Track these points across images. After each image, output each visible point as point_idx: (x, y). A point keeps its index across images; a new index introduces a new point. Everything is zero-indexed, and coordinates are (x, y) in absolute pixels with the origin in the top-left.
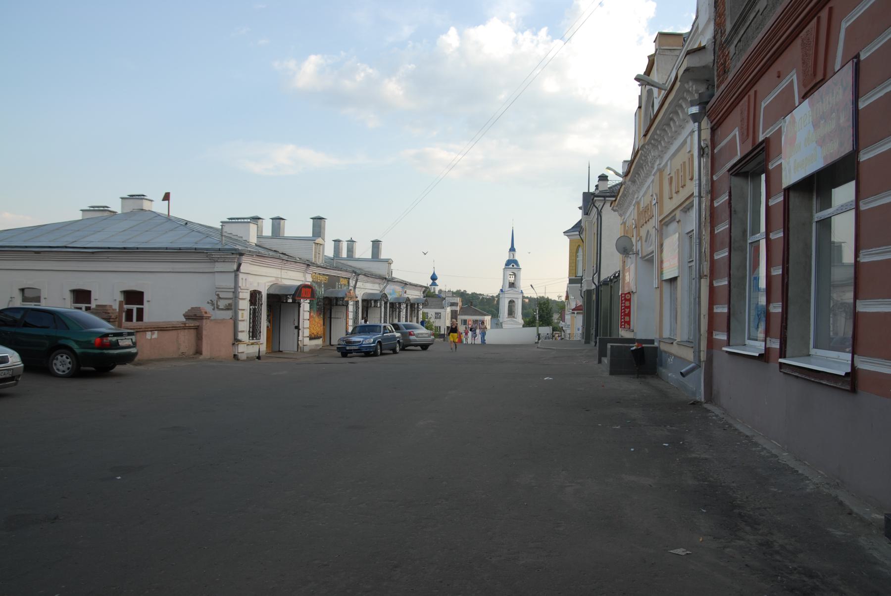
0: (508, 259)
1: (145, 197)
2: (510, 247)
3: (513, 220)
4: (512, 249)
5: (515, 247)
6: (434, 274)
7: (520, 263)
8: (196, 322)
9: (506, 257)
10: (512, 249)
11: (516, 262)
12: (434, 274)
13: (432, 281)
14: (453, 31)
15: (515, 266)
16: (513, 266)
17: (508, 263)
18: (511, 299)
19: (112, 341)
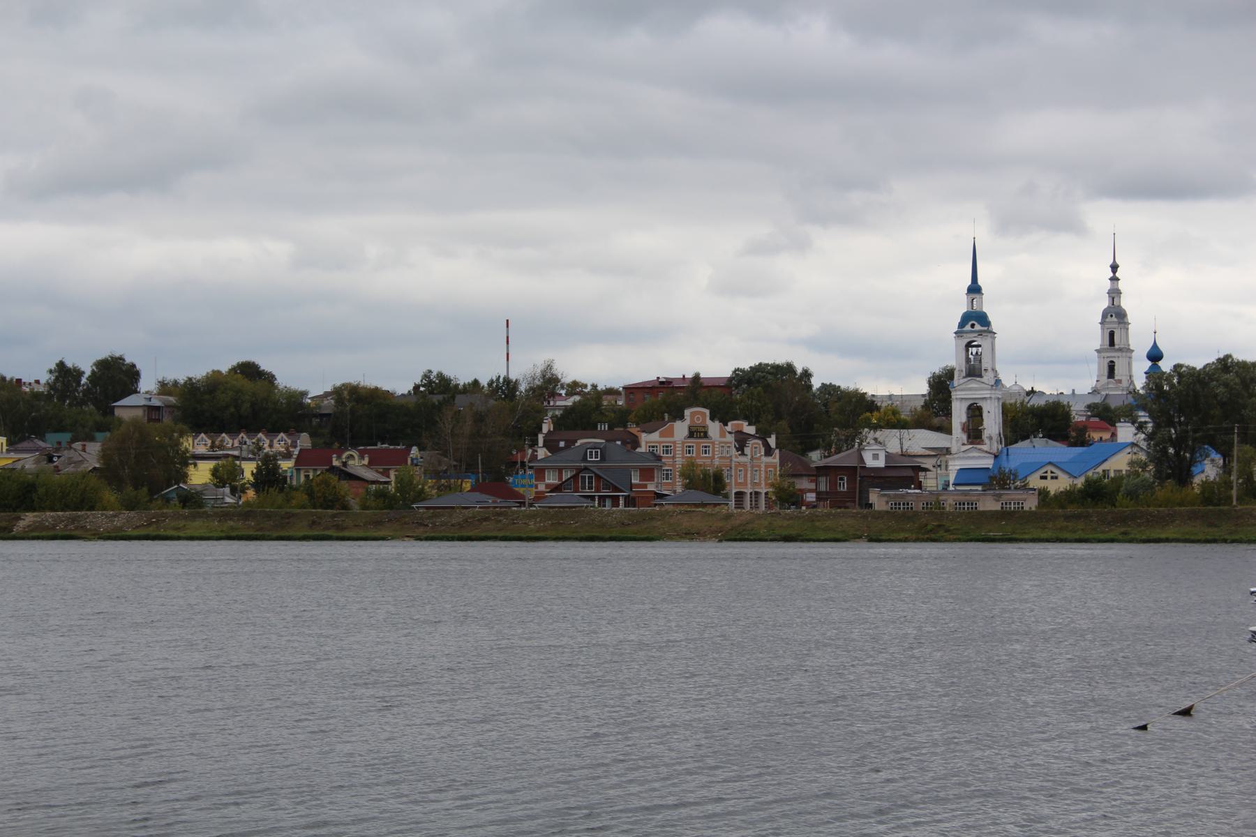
0: (966, 310)
1: (130, 717)
2: (970, 283)
3: (1114, 226)
4: (974, 289)
5: (980, 282)
6: (1155, 345)
7: (991, 318)
8: (1184, 722)
9: (962, 306)
10: (974, 289)
11: (982, 319)
12: (1155, 345)
13: (1149, 363)
14: (24, 388)
15: (978, 327)
16: (973, 326)
17: (966, 319)
18: (972, 402)
19: (89, 377)
